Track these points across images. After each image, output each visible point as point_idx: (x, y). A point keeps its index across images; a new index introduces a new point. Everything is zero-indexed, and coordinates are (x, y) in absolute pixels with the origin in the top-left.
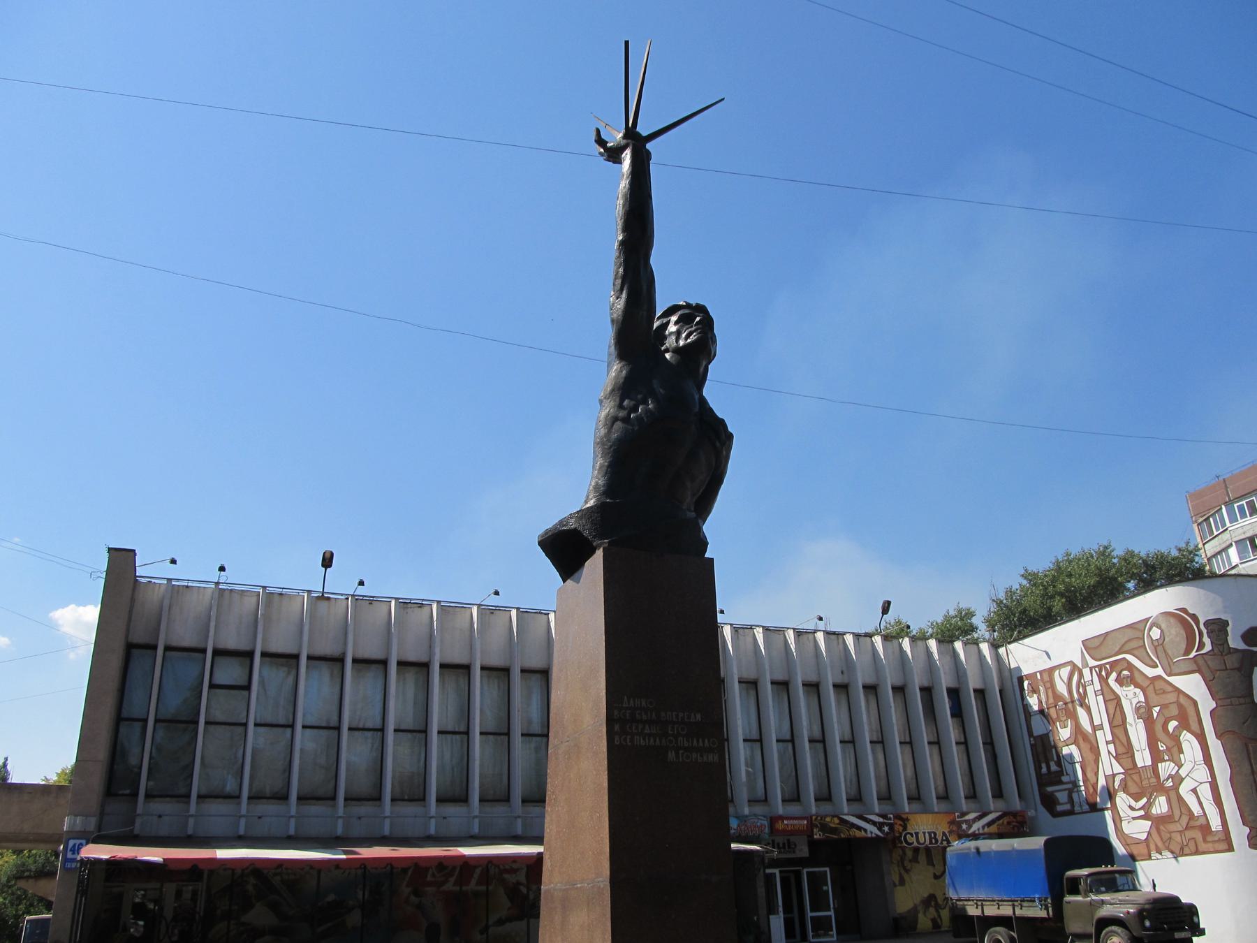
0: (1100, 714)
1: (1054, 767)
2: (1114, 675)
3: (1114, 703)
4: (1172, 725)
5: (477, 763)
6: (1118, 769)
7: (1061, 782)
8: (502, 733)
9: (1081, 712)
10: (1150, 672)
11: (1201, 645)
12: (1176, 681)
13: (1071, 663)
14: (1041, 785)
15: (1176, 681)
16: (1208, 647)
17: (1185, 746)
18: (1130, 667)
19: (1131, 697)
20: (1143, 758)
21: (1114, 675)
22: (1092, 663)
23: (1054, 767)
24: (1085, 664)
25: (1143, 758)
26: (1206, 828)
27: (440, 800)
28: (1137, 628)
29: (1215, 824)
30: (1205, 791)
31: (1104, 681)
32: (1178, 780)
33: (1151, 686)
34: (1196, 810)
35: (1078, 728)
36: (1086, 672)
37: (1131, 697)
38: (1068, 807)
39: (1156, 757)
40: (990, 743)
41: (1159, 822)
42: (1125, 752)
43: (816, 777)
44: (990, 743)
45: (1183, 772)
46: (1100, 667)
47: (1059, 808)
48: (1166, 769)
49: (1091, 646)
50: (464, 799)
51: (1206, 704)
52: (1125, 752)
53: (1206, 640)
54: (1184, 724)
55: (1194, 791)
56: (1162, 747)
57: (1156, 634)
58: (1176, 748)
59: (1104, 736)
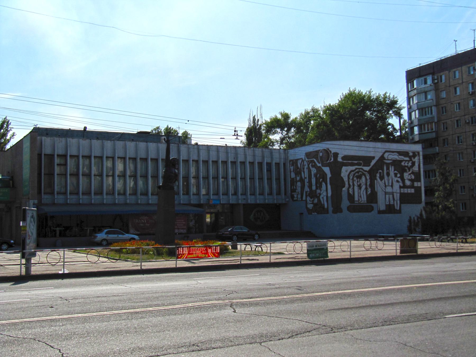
0: (307, 175)
1: (295, 187)
2: (311, 164)
3: (310, 171)
4: (321, 180)
5: (81, 186)
6: (308, 190)
7: (295, 192)
8: (134, 176)
9: (302, 173)
10: (319, 165)
11: (331, 159)
12: (323, 168)
13: (302, 159)
14: (291, 192)
15: (323, 168)
16: (332, 160)
17: (323, 186)
18: (315, 162)
19: (314, 171)
20: (314, 188)
21: (311, 164)
22: (307, 160)
23: (295, 187)
24: (305, 160)
25: (314, 188)
26: (324, 207)
27: (83, 194)
28: (317, 152)
29: (326, 206)
30: (325, 198)
31: (308, 165)
32: (320, 194)
33: (319, 169)
34: (322, 202)
35: (301, 177)
36: (305, 162)
37: (314, 171)
38: (296, 199)
39: (317, 188)
40: (278, 179)
41: (315, 205)
42: (310, 186)
43: (251, 188)
44: (278, 179)
45: (321, 192)
46: (308, 161)
47: (295, 199)
48: (318, 191)
49: (308, 155)
50: (101, 193)
51: (329, 175)
52: (310, 186)
53: (332, 158)
54: (323, 181)
55: (323, 198)
56: (318, 185)
57: (321, 154)
58: (321, 187)
59: (306, 180)
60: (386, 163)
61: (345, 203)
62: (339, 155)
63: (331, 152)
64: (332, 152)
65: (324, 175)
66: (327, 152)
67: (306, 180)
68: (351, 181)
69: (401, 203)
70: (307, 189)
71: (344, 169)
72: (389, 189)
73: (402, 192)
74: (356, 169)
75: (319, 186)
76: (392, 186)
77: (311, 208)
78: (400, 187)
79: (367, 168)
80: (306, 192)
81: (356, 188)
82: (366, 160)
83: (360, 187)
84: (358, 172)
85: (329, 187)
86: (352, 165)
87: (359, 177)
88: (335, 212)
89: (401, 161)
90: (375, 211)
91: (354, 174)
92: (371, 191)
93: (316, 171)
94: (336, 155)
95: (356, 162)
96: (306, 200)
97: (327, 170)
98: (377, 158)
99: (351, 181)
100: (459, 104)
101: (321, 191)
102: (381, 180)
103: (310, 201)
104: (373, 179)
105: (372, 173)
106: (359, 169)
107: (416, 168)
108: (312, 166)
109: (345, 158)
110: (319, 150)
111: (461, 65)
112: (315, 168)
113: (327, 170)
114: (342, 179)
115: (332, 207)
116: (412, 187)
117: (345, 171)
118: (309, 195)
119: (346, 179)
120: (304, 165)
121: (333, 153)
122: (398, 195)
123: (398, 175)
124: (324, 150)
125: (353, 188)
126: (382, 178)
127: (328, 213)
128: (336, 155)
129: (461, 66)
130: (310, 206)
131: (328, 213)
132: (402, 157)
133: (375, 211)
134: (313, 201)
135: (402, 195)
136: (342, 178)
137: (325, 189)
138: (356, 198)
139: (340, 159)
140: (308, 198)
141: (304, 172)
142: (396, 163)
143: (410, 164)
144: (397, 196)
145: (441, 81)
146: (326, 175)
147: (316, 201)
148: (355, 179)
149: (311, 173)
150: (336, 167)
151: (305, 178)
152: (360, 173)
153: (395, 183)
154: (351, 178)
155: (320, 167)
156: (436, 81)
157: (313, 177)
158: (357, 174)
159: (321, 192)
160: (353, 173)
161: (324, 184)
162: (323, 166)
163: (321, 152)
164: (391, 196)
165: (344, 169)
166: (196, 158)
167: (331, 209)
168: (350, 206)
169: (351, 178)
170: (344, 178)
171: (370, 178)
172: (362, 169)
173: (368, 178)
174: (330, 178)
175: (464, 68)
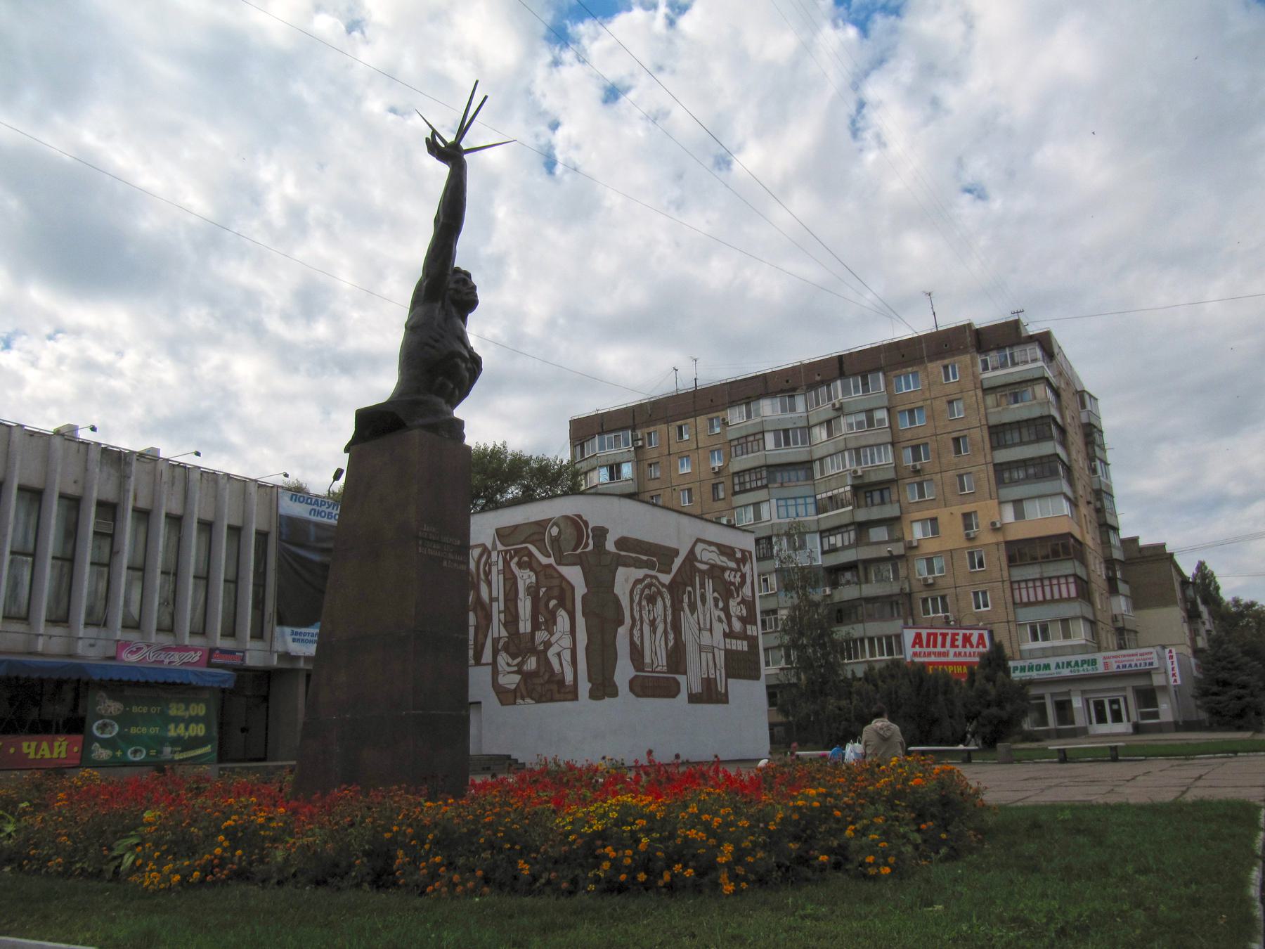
2: (516, 559)
4: (553, 603)
6: (504, 633)
10: (544, 560)
11: (587, 545)
13: (483, 545)
16: (591, 547)
17: (559, 620)
18: (530, 555)
19: (525, 578)
20: (525, 626)
21: (516, 559)
22: (500, 547)
24: (495, 548)
25: (525, 626)
26: (561, 682)
28: (542, 525)
29: (569, 678)
30: (567, 656)
31: (507, 563)
32: (548, 645)
33: (545, 573)
34: (556, 667)
36: (494, 555)
37: (525, 578)
39: (536, 626)
41: (527, 677)
42: (512, 619)
45: (553, 639)
46: (506, 552)
48: (541, 636)
51: (580, 590)
52: (512, 619)
53: (591, 542)
54: (562, 604)
55: (559, 654)
56: (541, 619)
57: (555, 531)
58: (552, 620)
59: (497, 609)
60: (700, 571)
61: (624, 672)
62: (608, 536)
63: (586, 523)
64: (590, 526)
65: (564, 593)
66: (576, 523)
67: (497, 609)
68: (636, 608)
69: (727, 676)
70: (497, 629)
71: (621, 572)
72: (706, 639)
73: (728, 647)
74: (646, 576)
75: (544, 618)
76: (711, 630)
77: (513, 687)
78: (726, 635)
79: (666, 579)
80: (496, 641)
81: (646, 628)
82: (662, 555)
83: (653, 623)
84: (649, 586)
85: (580, 621)
86: (638, 564)
87: (652, 600)
88: (595, 695)
89: (723, 569)
90: (683, 695)
91: (643, 591)
92: (675, 639)
93: (534, 579)
94: (601, 533)
95: (645, 558)
96: (494, 664)
97: (574, 574)
98: (683, 554)
99: (636, 608)
100: (690, 490)
101: (552, 634)
102: (692, 614)
103: (508, 665)
104: (677, 608)
105: (675, 588)
106: (652, 577)
107: (747, 590)
108: (520, 565)
109: (622, 543)
110: (550, 520)
111: (696, 413)
112: (532, 569)
113: (574, 574)
114: (616, 601)
115: (590, 680)
116: (743, 636)
117: (625, 579)
118: (506, 649)
119: (625, 602)
120: (488, 564)
121: (594, 529)
122: (722, 653)
123: (721, 605)
124: (567, 518)
125: (641, 629)
126: (693, 608)
127: (576, 698)
128: (601, 533)
129: (695, 416)
130: (510, 680)
131: (576, 698)
132: (724, 559)
133: (683, 695)
134: (520, 665)
135: (729, 654)
136: (616, 597)
137: (567, 627)
138: (647, 660)
139: (610, 546)
140: (503, 659)
141: (489, 584)
142: (715, 572)
143: (738, 579)
144: (721, 657)
145: (650, 444)
146: (573, 588)
147: (531, 664)
148: (644, 603)
149: (515, 583)
150: (600, 571)
151: (492, 599)
152: (653, 589)
153: (716, 624)
154: (637, 599)
155: (550, 566)
156: (640, 443)
157: (521, 594)
158: (647, 591)
159: (553, 639)
160: (640, 586)
161: (562, 618)
162: (559, 564)
163: (556, 524)
164: (710, 656)
165: (621, 572)
166: (176, 509)
167: (584, 687)
168: (636, 677)
169: (637, 599)
170: (621, 598)
171: (673, 605)
172: (656, 578)
173: (668, 603)
174: (584, 597)
175: (702, 421)
